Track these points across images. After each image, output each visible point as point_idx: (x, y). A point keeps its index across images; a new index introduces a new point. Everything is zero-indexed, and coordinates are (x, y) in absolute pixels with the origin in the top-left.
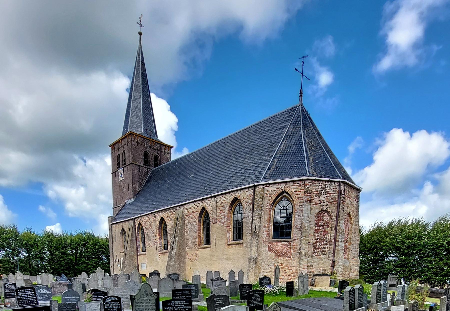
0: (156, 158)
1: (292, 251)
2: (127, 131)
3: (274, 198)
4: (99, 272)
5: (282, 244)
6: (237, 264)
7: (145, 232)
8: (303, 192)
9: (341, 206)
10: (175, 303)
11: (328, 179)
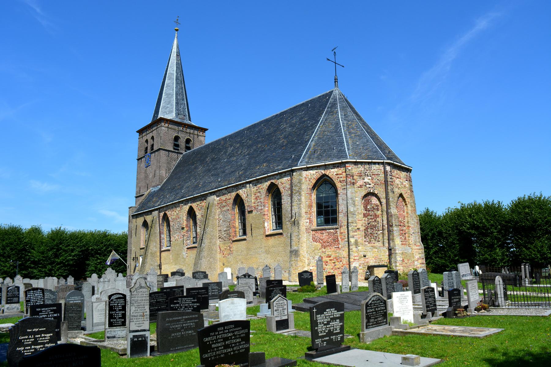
0: (188, 141)
1: (340, 239)
2: (157, 116)
3: (314, 182)
4: (110, 273)
5: (328, 233)
6: (278, 258)
7: (171, 223)
8: (344, 174)
11: (370, 161)
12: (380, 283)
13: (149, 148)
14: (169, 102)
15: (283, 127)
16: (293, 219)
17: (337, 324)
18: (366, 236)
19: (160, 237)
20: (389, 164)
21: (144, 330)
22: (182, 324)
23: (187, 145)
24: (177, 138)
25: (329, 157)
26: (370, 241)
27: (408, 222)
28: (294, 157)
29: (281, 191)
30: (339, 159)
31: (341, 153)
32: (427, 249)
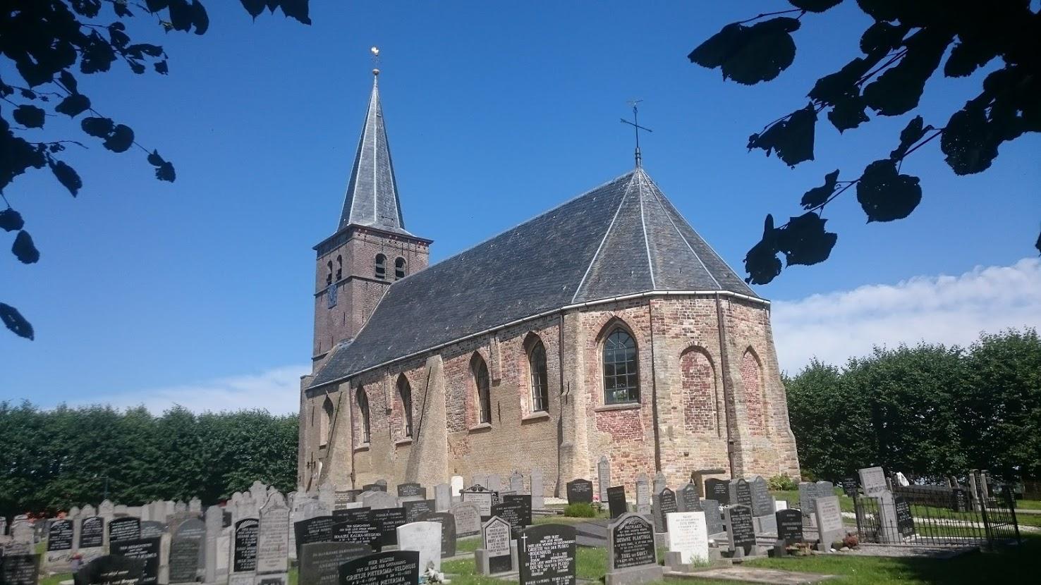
0: (399, 262)
1: (643, 426)
2: (347, 222)
3: (598, 330)
7: (369, 402)
9: (726, 337)
10: (352, 528)
11: (693, 292)
12: (673, 499)
13: (334, 277)
14: (367, 197)
15: (550, 237)
16: (564, 394)
17: (563, 561)
18: (688, 420)
19: (353, 425)
20: (726, 297)
21: (280, 572)
22: (339, 562)
23: (399, 269)
24: (380, 258)
25: (624, 288)
26: (696, 429)
27: (764, 396)
28: (566, 290)
29: (546, 346)
30: (638, 291)
31: (644, 281)
32: (802, 442)
